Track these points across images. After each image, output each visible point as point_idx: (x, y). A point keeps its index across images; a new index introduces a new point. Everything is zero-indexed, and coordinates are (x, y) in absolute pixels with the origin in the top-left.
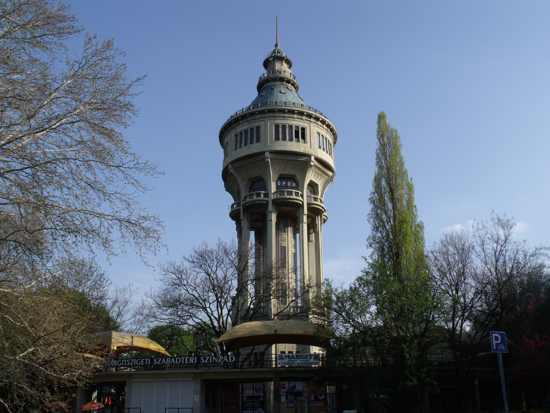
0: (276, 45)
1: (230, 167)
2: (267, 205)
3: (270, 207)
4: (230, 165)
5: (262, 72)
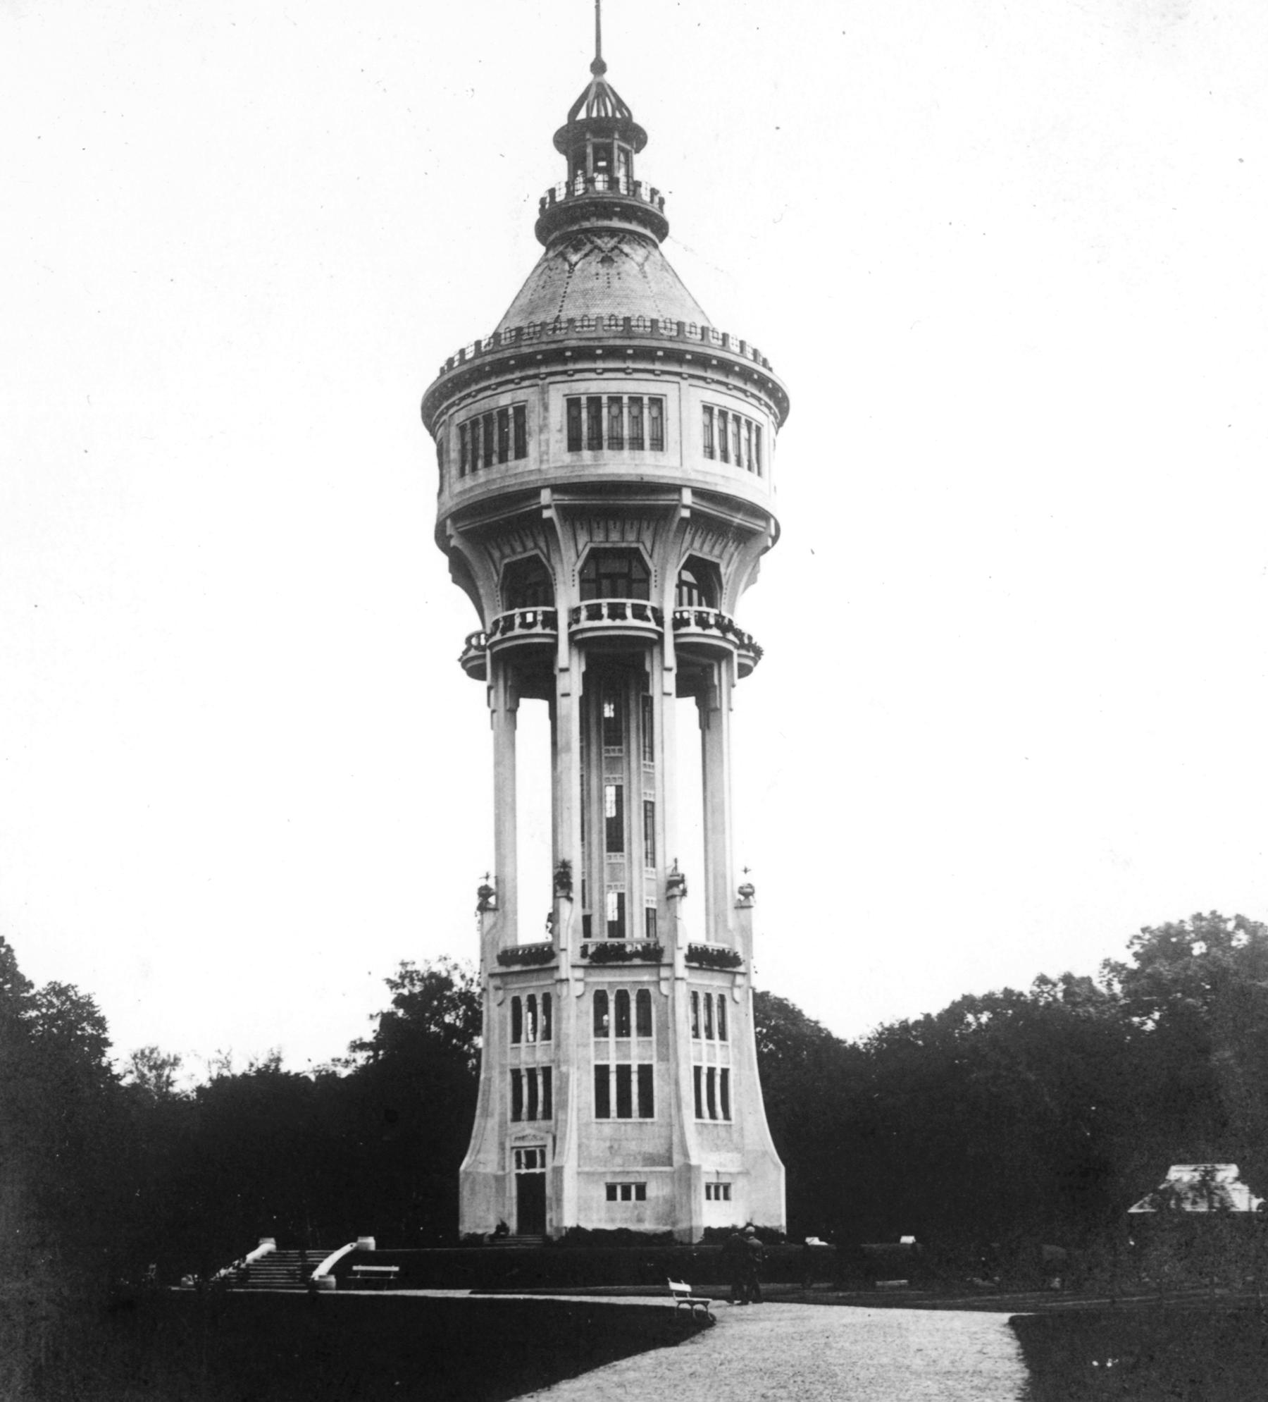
0: (598, 67)
1: (450, 530)
2: (554, 648)
3: (564, 656)
4: (449, 522)
5: (553, 172)
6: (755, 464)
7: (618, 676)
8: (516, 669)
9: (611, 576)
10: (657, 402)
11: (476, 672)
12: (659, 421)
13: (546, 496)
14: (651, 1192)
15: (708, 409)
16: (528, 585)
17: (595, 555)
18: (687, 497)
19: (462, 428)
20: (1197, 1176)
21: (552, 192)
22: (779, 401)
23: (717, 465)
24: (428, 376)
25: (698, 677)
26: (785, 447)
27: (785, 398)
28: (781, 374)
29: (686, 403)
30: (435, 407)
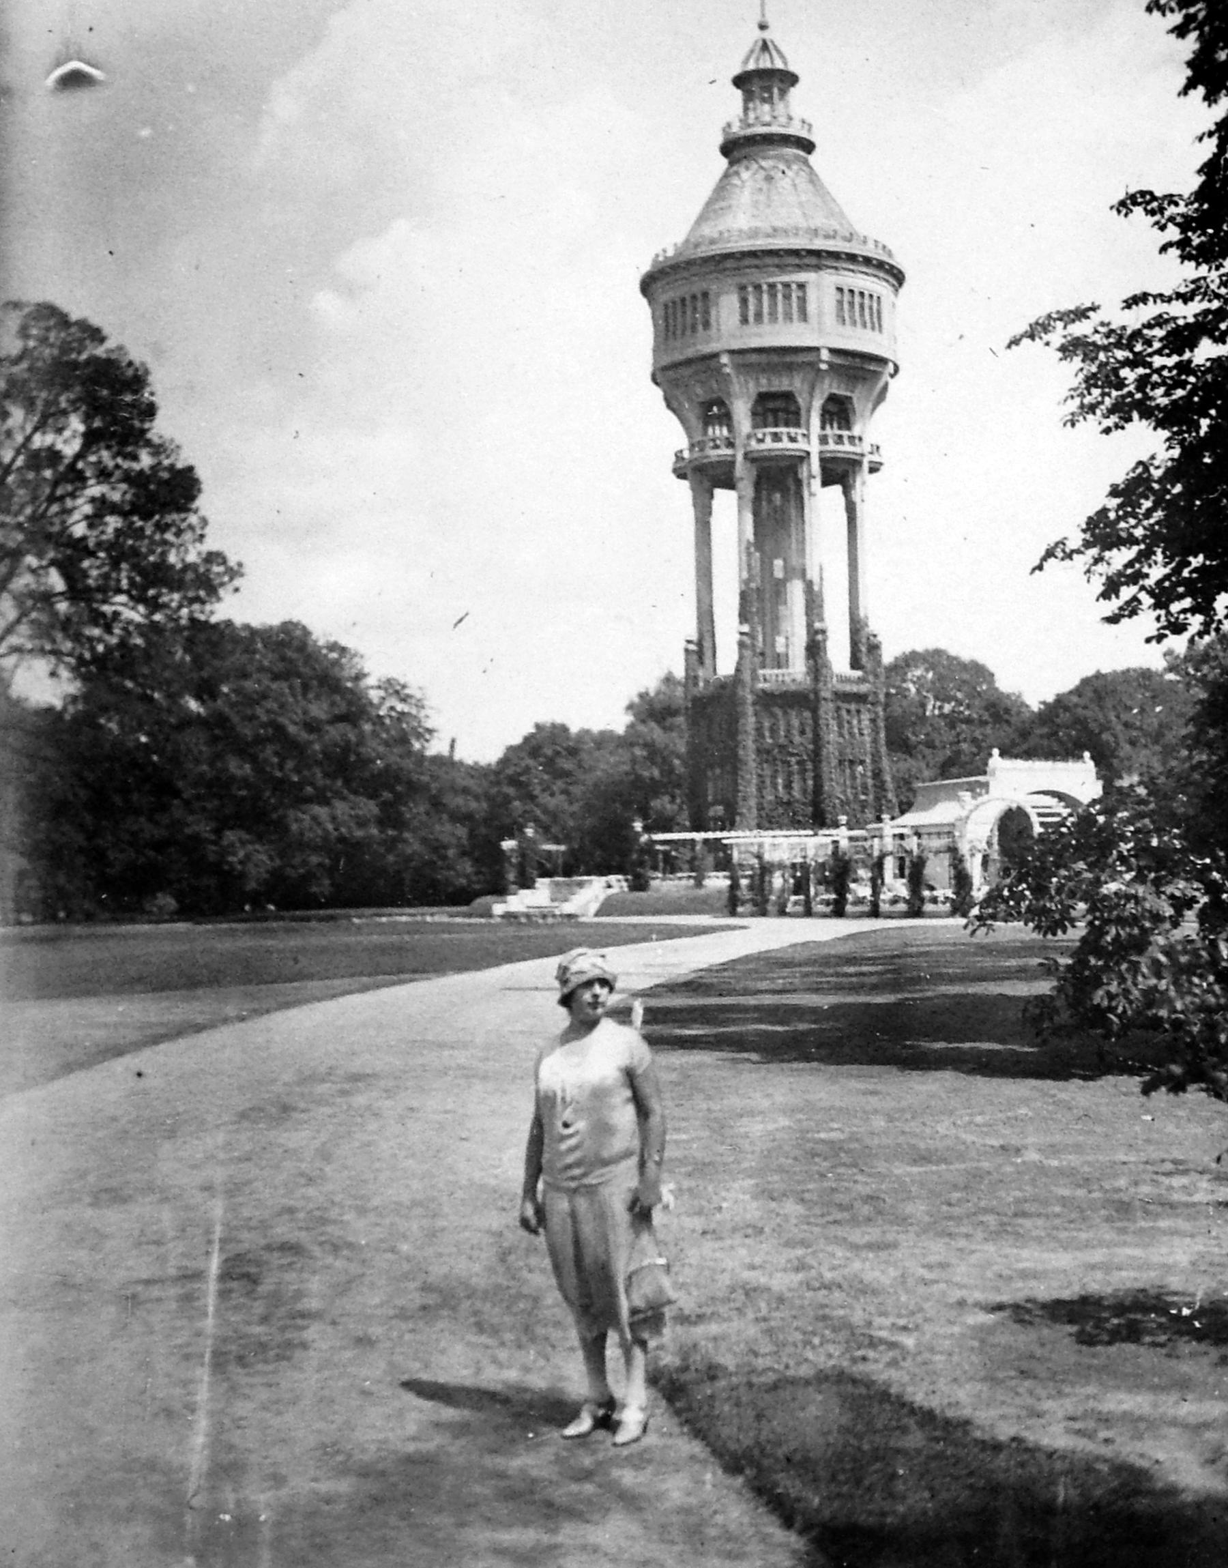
6: (876, 323)
7: (777, 485)
8: (705, 476)
9: (775, 411)
10: (801, 286)
11: (681, 475)
12: (803, 301)
13: (725, 359)
14: (1128, 747)
15: (840, 290)
16: (714, 411)
17: (763, 398)
18: (825, 355)
19: (666, 306)
20: (706, 882)
21: (729, 125)
22: (897, 277)
23: (848, 329)
24: (646, 267)
25: (839, 472)
26: (900, 308)
27: (900, 272)
28: (899, 261)
29: (822, 286)
30: (648, 286)
